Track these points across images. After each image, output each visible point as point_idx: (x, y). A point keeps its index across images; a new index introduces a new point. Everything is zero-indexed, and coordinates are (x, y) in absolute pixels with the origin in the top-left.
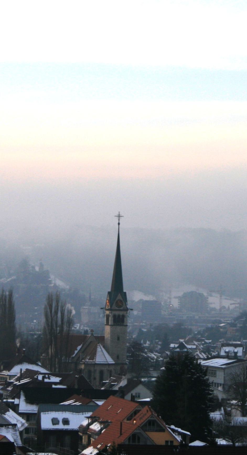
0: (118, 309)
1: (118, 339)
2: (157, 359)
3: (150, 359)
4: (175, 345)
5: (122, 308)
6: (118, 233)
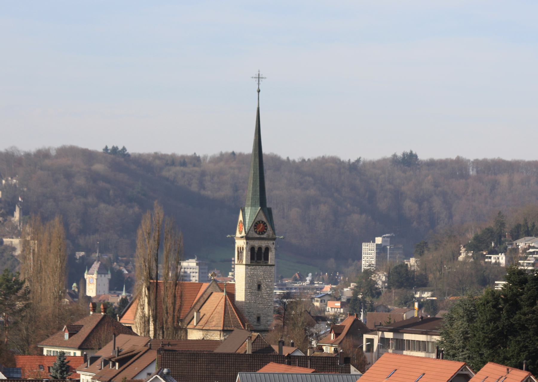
0: (258, 236)
1: (259, 287)
2: (494, 297)
3: (124, 325)
4: (75, 351)
5: (265, 236)
6: (257, 106)
